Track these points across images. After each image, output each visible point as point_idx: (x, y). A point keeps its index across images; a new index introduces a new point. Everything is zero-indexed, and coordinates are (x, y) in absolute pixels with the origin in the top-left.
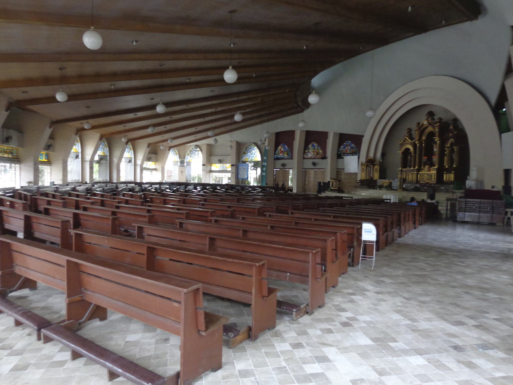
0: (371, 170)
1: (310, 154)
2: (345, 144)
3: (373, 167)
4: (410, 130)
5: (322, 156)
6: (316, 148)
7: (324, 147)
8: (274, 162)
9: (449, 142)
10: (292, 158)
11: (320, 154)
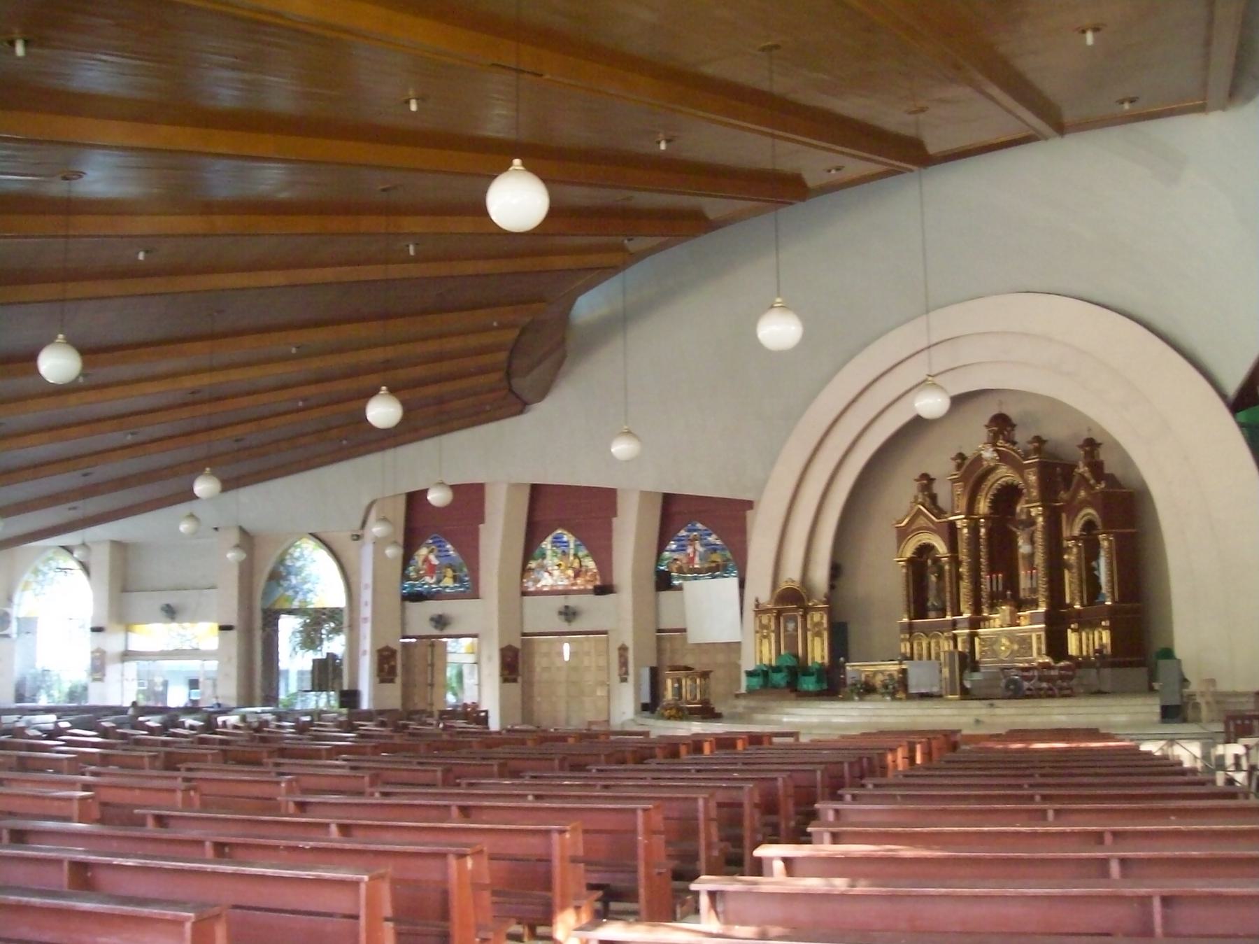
0: (796, 630)
1: (546, 574)
2: (683, 533)
3: (804, 617)
4: (927, 482)
5: (598, 583)
6: (572, 552)
7: (601, 548)
8: (403, 610)
9: (1077, 520)
10: (473, 593)
11: (589, 574)
